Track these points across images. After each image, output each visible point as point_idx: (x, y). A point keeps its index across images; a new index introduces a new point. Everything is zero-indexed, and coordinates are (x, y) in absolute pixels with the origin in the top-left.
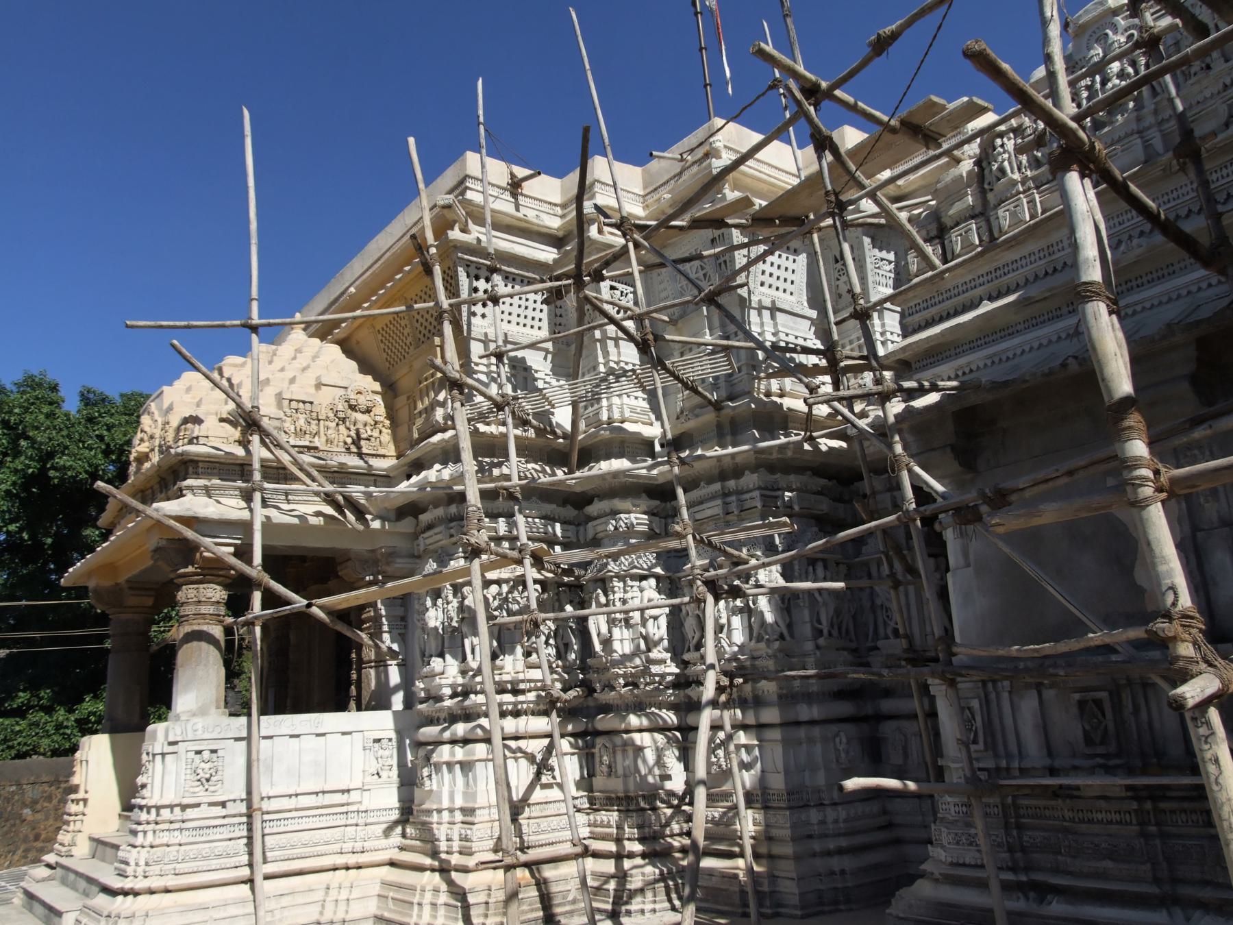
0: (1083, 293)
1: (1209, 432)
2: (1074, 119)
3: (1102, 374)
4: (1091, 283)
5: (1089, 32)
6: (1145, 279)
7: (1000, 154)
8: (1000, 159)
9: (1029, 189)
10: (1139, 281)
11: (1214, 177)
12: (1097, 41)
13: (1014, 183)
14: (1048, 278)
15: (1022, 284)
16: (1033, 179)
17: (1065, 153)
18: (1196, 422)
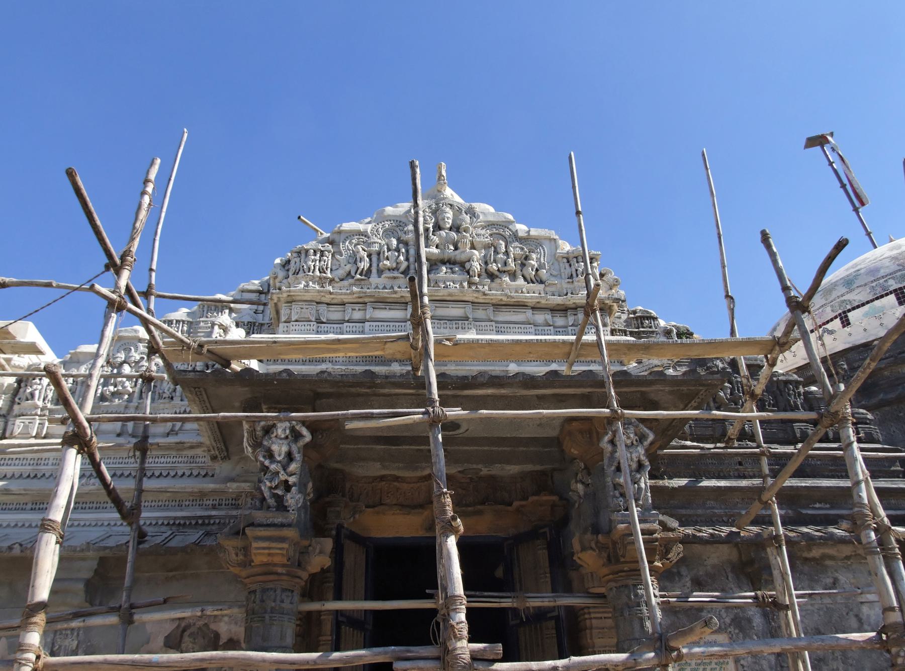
0: (46, 526)
1: (82, 624)
2: (89, 421)
3: (34, 581)
4: (53, 521)
5: (122, 342)
6: (88, 506)
7: (36, 384)
8: (35, 387)
9: (44, 415)
10: (84, 505)
11: (151, 460)
12: (125, 350)
13: (36, 407)
14: (28, 480)
15: (8, 476)
16: (51, 411)
17: (77, 439)
18: (76, 615)
